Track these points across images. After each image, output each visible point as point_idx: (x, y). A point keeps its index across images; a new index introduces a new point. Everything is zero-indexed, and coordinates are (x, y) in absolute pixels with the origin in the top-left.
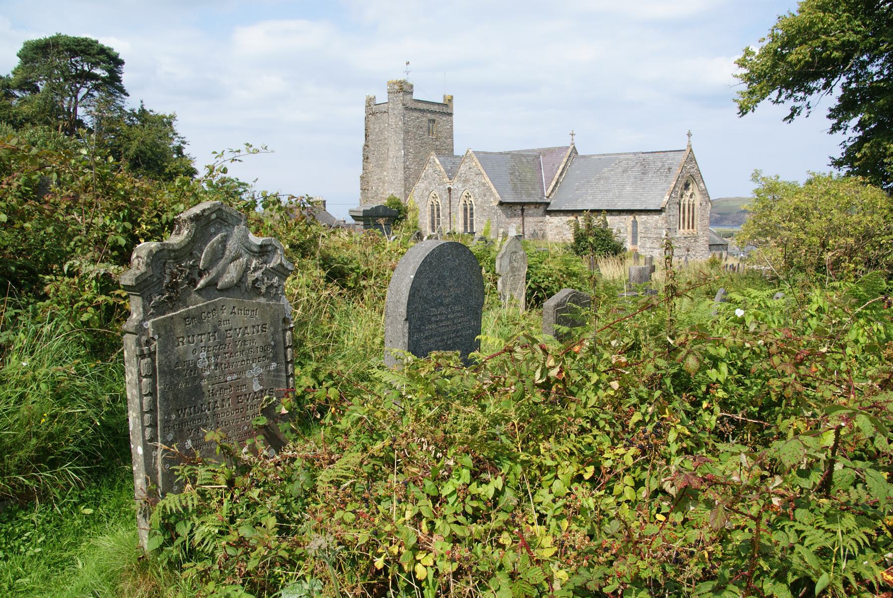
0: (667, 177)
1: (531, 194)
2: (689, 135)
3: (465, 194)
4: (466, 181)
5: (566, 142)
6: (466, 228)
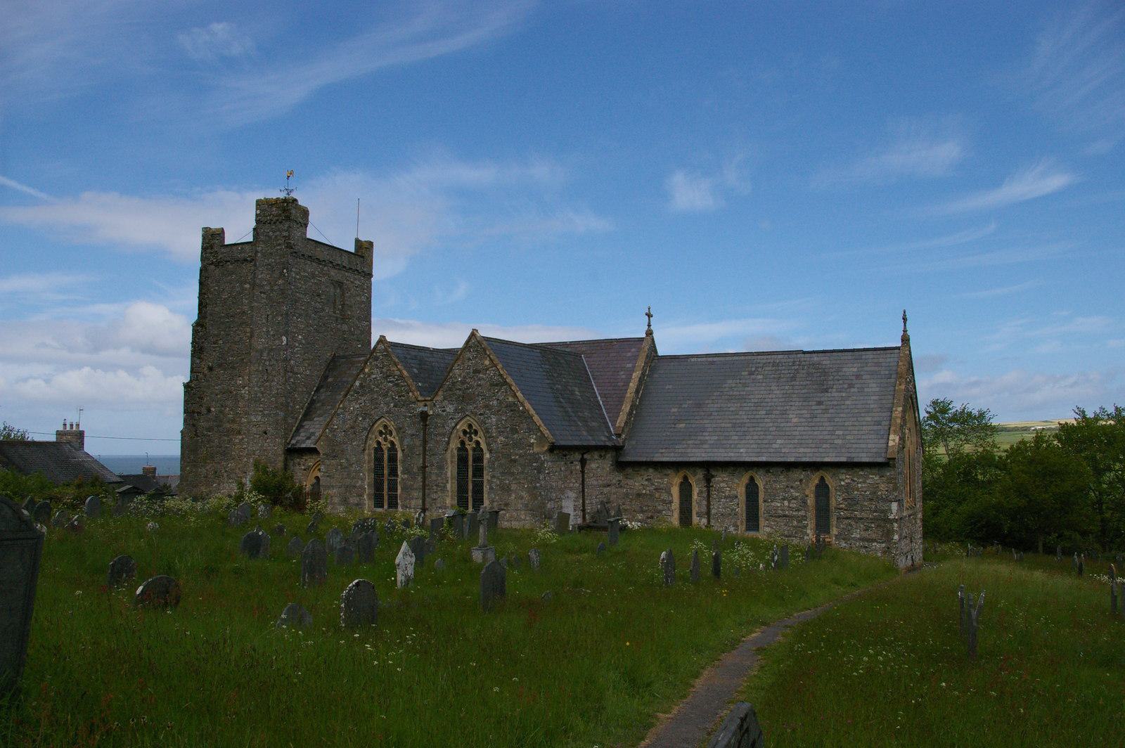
3: (462, 426)
6: (462, 501)
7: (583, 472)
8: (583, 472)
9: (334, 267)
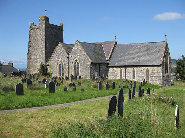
0: (159, 52)
1: (102, 59)
2: (166, 36)
4: (76, 54)
5: (113, 40)
7: (99, 68)
8: (99, 68)
9: (55, 29)
